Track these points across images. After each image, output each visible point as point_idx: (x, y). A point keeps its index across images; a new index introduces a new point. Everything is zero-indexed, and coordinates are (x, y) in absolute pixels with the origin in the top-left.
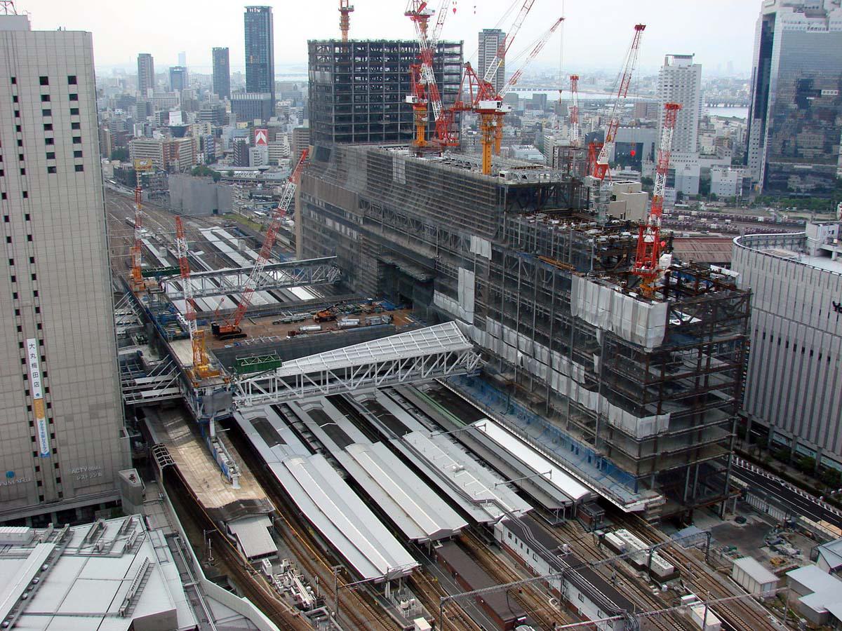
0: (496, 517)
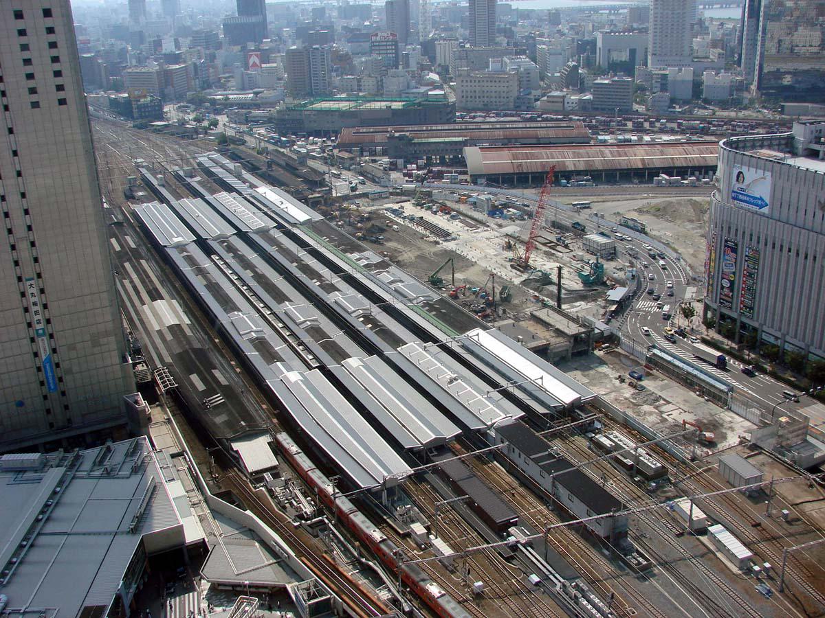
0: (489, 423)
